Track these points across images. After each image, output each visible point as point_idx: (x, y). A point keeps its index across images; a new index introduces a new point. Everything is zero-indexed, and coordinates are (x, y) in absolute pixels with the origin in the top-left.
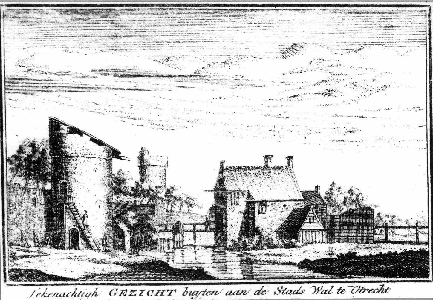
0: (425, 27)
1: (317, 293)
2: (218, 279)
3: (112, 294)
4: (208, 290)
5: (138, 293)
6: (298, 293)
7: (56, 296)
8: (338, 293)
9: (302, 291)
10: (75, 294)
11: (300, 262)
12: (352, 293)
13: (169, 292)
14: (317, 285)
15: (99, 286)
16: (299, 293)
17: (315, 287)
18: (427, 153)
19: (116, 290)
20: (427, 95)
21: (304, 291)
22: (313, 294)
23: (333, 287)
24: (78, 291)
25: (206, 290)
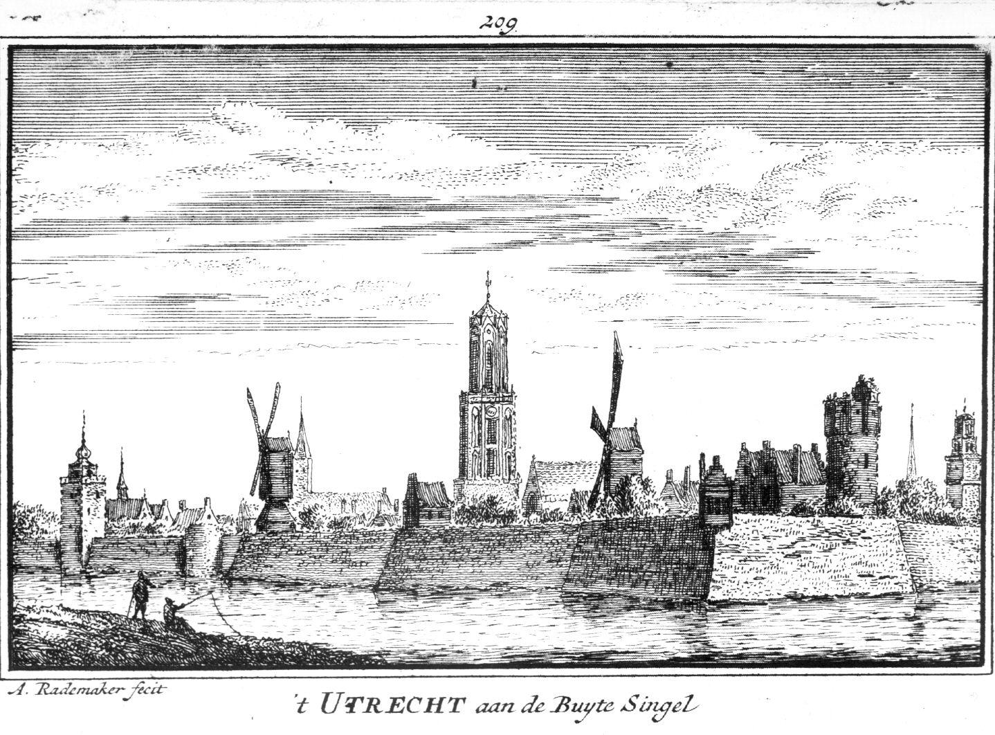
8: (512, 704)
12: (654, 720)
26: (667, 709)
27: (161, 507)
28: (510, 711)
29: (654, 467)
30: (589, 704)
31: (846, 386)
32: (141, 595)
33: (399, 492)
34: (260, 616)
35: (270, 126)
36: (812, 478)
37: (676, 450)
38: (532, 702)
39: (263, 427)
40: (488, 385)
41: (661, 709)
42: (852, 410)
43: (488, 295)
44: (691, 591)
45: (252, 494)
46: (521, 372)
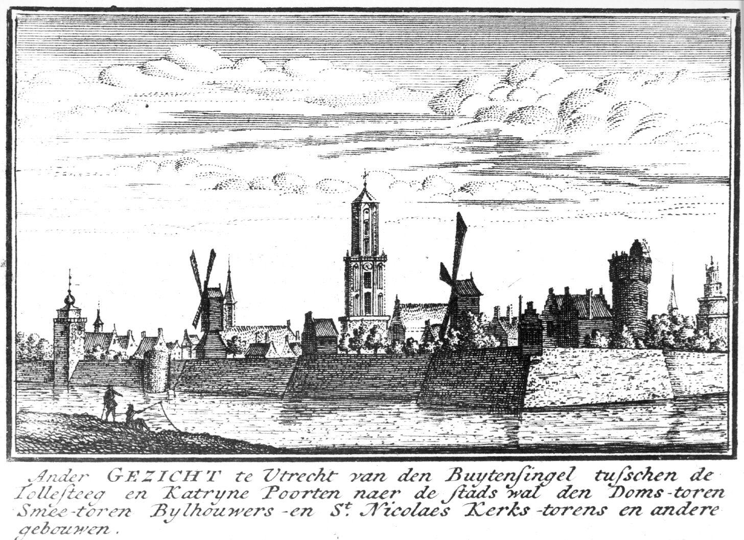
0: (17, 44)
3: (113, 477)
4: (498, 471)
5: (157, 475)
7: (362, 497)
8: (429, 474)
9: (493, 492)
11: (535, 310)
18: (731, 119)
19: (628, 468)
20: (731, 86)
21: (606, 508)
22: (229, 515)
23: (574, 468)
25: (495, 471)
26: (551, 479)
27: (127, 337)
28: (586, 497)
29: (486, 307)
30: (219, 492)
31: (626, 248)
32: (110, 402)
33: (299, 326)
34: (191, 414)
35: (202, 59)
36: (614, 309)
37: (509, 285)
38: (407, 473)
39: (203, 279)
40: (364, 261)
41: (546, 479)
42: (628, 267)
43: (365, 184)
44: (509, 399)
45: (195, 325)
46: (388, 242)
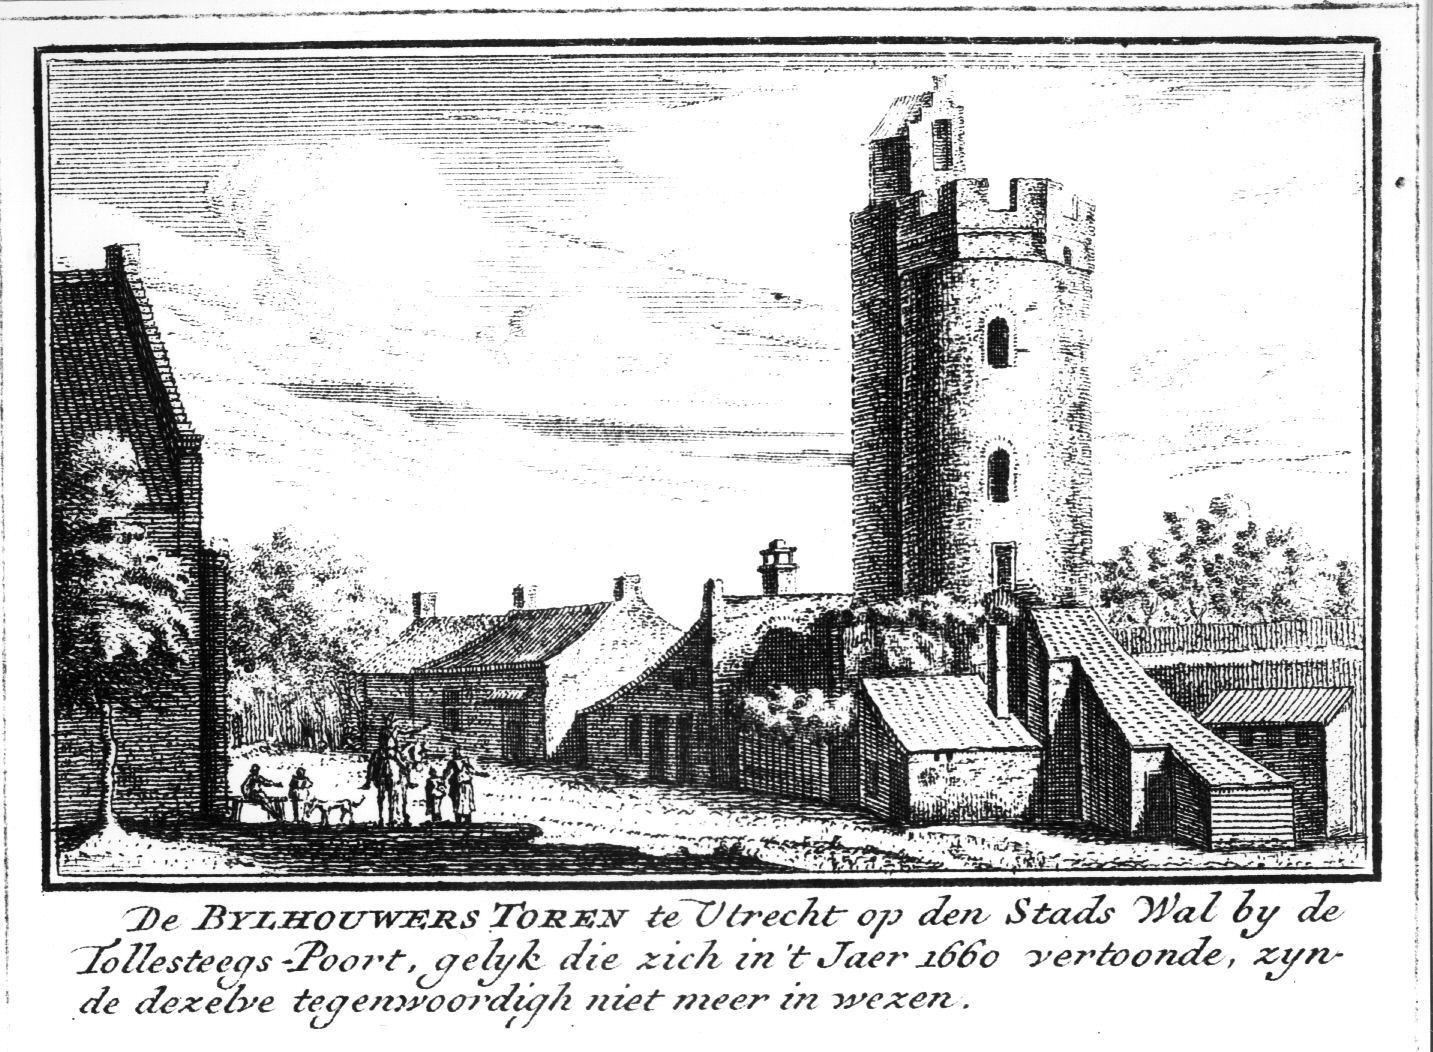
1: (1155, 920)
2: (796, 870)
6: (1093, 919)
10: (811, 915)
13: (503, 910)
14: (1158, 892)
15: (1113, 888)
16: (1098, 920)
17: (1150, 901)
23: (1218, 894)
24: (822, 908)
